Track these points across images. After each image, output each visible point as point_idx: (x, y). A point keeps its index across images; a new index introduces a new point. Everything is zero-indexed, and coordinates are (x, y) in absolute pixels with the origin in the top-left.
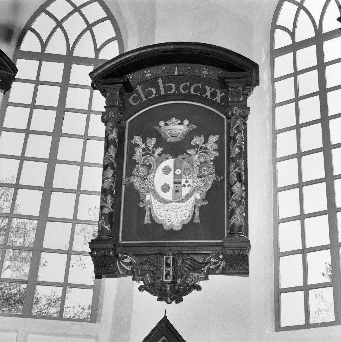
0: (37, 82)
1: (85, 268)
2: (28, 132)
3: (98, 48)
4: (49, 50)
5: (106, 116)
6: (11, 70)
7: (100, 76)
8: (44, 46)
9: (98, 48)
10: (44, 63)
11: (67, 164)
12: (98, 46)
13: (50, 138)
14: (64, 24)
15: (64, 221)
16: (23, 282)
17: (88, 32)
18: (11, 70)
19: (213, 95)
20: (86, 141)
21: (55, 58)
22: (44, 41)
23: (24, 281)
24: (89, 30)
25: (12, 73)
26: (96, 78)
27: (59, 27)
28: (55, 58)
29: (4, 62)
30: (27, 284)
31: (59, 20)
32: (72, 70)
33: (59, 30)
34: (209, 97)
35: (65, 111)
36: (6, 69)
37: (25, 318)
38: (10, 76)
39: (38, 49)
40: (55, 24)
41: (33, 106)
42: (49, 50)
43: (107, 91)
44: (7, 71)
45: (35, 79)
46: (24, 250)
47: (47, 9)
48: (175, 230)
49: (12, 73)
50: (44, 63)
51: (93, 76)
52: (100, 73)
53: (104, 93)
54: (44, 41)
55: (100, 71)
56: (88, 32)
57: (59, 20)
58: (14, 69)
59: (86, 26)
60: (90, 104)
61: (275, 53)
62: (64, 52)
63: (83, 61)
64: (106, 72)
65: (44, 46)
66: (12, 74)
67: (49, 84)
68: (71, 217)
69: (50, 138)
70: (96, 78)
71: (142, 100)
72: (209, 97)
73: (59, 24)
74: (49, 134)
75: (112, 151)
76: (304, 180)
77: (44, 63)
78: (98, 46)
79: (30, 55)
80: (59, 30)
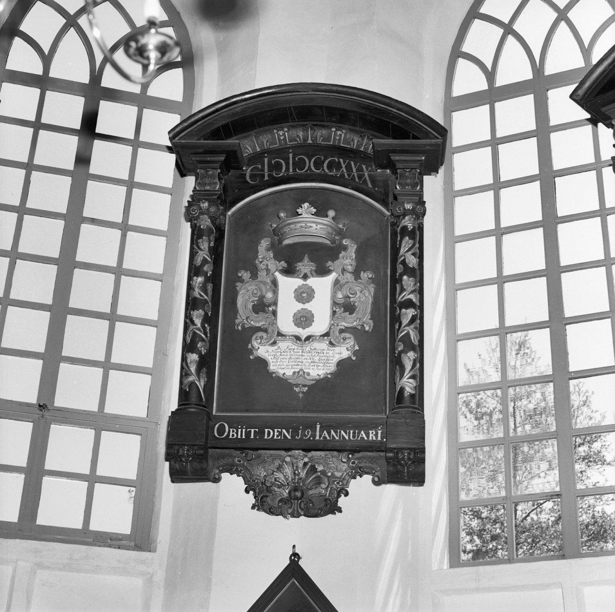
0: (494, 142)
2: (499, 232)
3: (586, 47)
4: (501, 80)
5: (423, 158)
6: (436, 134)
7: (590, 93)
8: (490, 75)
9: (586, 47)
10: (497, 105)
11: (582, 269)
12: (586, 42)
13: (540, 231)
14: (516, 27)
15: (602, 372)
16: (551, 496)
17: (563, 24)
18: (436, 134)
20: (606, 219)
21: (515, 90)
22: (489, 67)
23: (553, 494)
24: (562, 20)
25: (438, 138)
26: (584, 99)
27: (509, 33)
28: (515, 90)
29: (422, 124)
30: (560, 498)
31: (507, 22)
32: (550, 102)
33: (511, 39)
35: (554, 178)
36: (427, 135)
37: (569, 560)
38: (437, 145)
39: (481, 84)
41: (497, 186)
43: (612, 117)
44: (430, 139)
46: (534, 440)
47: (481, 11)
49: (438, 138)
51: (578, 98)
52: (589, 88)
53: (608, 122)
55: (587, 85)
56: (563, 24)
57: (507, 22)
58: (440, 131)
59: (555, 15)
62: (528, 75)
63: (559, 79)
64: (600, 82)
65: (490, 75)
66: (440, 141)
67: (517, 137)
68: (98, 486)
69: (540, 231)
70: (584, 99)
73: (508, 29)
75: (205, 245)
76: (499, 134)
77: (497, 105)
78: (586, 42)
79: (471, 100)
80: (511, 39)
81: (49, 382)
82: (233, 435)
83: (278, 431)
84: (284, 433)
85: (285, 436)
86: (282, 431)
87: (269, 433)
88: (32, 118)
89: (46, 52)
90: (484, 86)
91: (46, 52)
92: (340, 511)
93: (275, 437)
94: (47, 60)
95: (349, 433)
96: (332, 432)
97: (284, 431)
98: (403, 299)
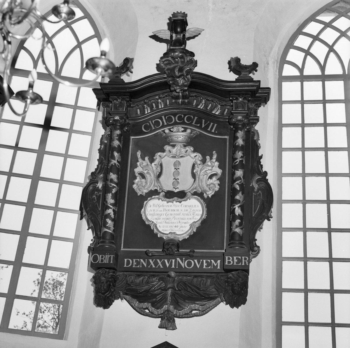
1: (155, 37)
4: (306, 73)
8: (323, 68)
14: (335, 48)
19: (156, 263)
22: (322, 64)
33: (332, 54)
34: (158, 260)
40: (303, 54)
42: (306, 73)
45: (300, 98)
48: (164, 43)
50: (304, 83)
54: (322, 64)
60: (327, 167)
61: (282, 79)
65: (323, 68)
71: (192, 123)
72: (158, 260)
74: (346, 231)
81: (43, 141)
82: (229, 262)
83: (206, 262)
84: (178, 261)
85: (142, 264)
86: (140, 260)
87: (128, 262)
88: (299, 99)
89: (301, 67)
90: (319, 73)
91: (301, 67)
92: (159, 327)
93: (134, 266)
94: (301, 70)
95: (175, 266)
96: (145, 265)
97: (142, 260)
98: (220, 176)
